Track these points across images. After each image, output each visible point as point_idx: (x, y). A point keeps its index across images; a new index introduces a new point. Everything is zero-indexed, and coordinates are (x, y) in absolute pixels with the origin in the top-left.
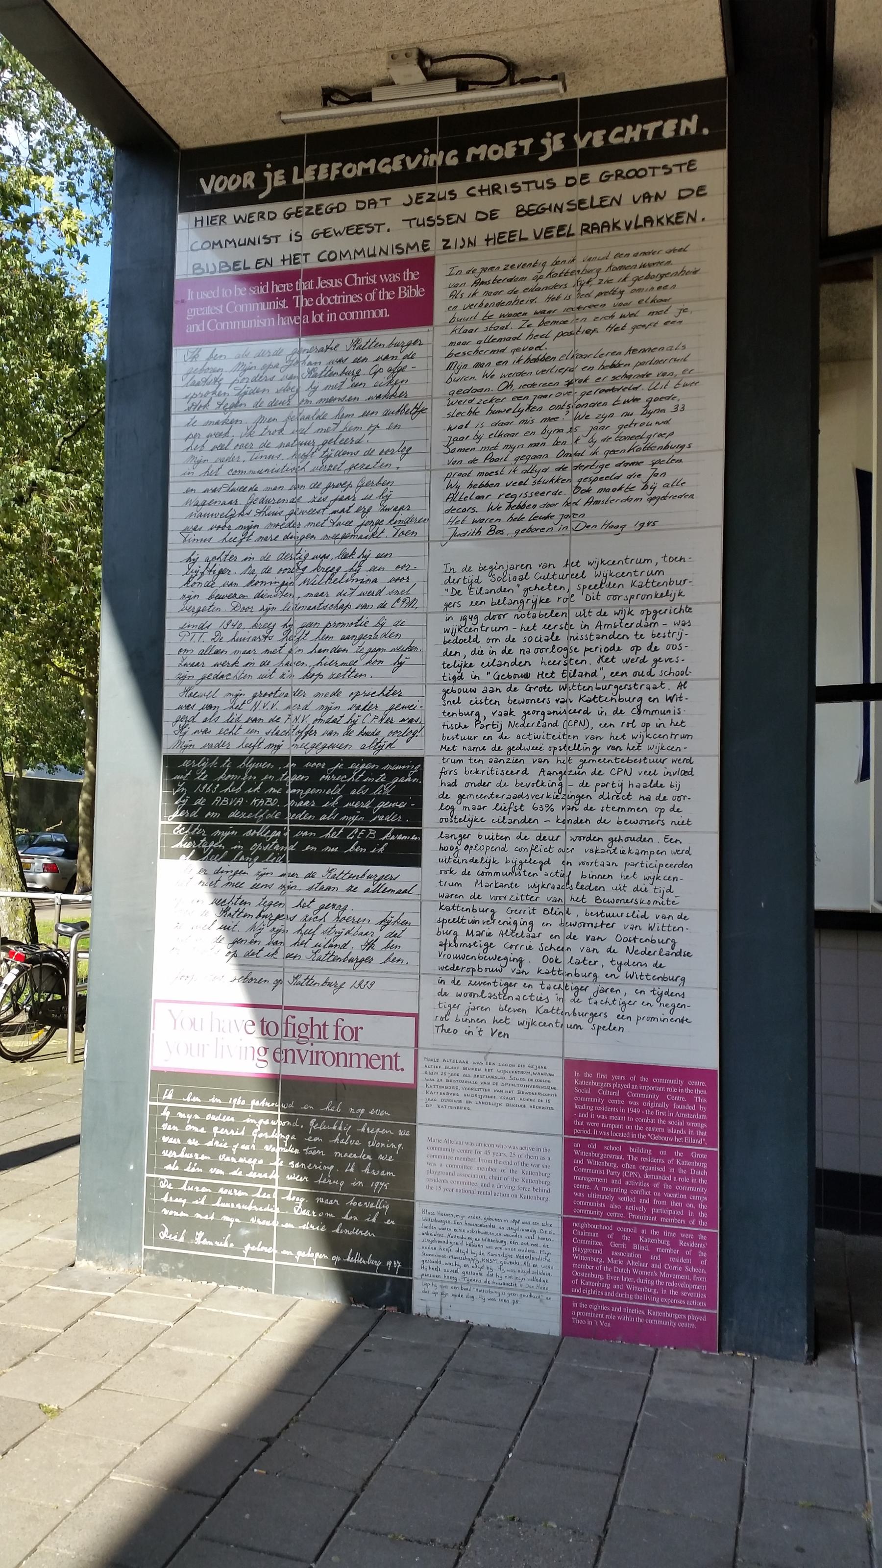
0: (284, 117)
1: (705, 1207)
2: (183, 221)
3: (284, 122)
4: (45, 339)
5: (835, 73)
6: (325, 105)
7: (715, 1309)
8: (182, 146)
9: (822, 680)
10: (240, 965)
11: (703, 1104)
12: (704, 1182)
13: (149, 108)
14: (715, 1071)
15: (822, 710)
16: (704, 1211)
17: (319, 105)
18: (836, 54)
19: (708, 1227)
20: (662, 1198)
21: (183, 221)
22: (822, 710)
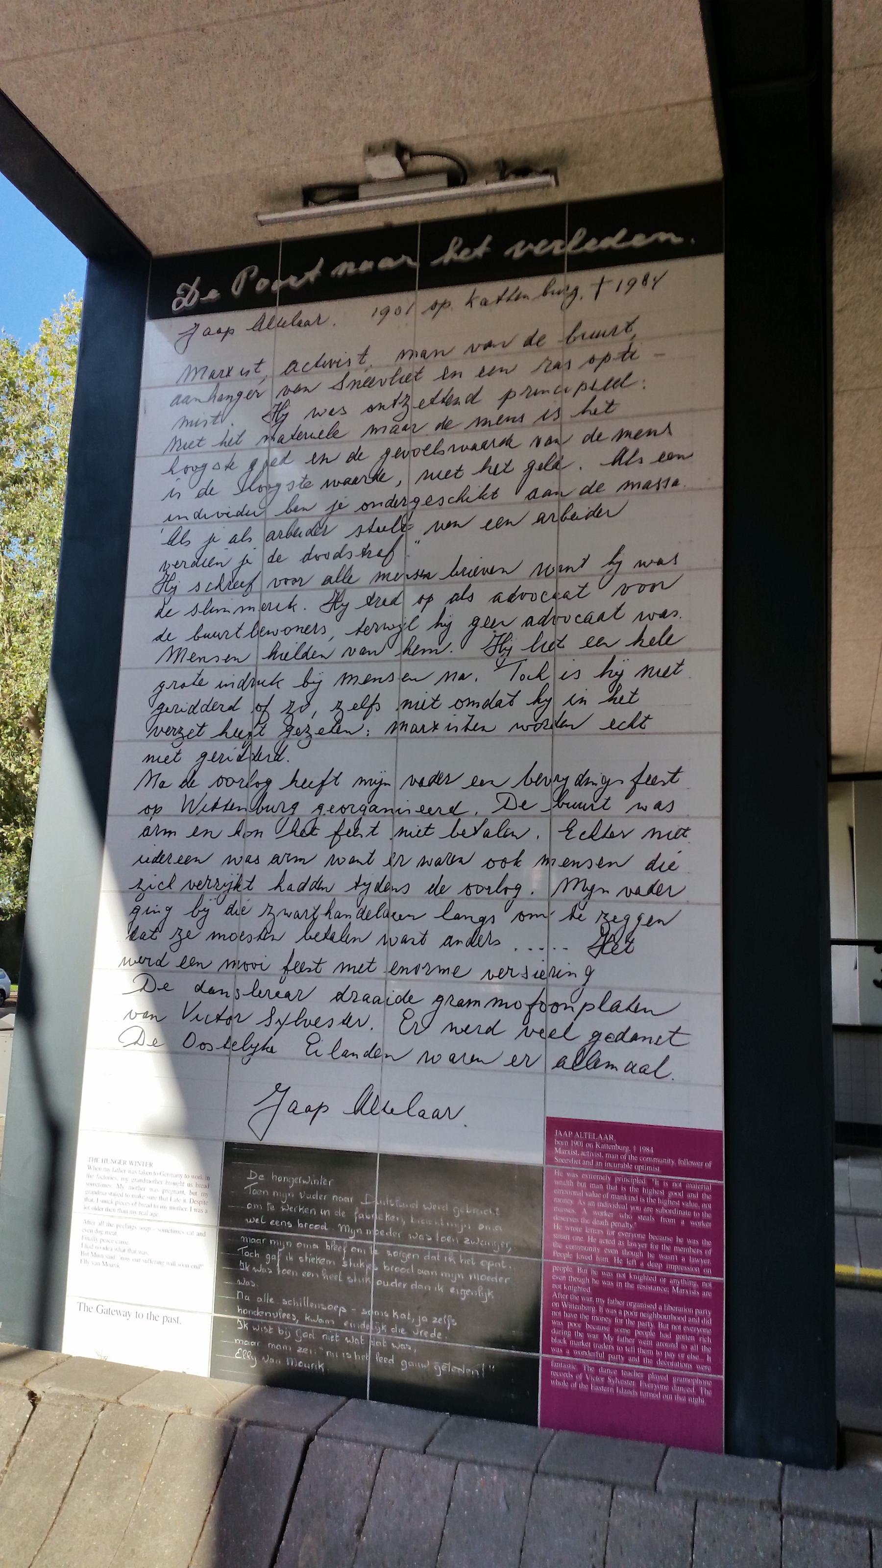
0: (261, 218)
1: (709, 1197)
2: (152, 328)
3: (261, 223)
4: (75, 1418)
5: (835, 164)
6: (306, 205)
7: (722, 1374)
8: (154, 253)
9: (834, 936)
10: (138, 949)
11: (707, 1267)
12: (709, 1216)
13: (125, 219)
14: (718, 1133)
15: (834, 948)
16: (708, 1212)
17: (300, 203)
18: (833, 151)
19: (712, 1373)
20: (657, 1260)
21: (152, 328)
22: (834, 948)
